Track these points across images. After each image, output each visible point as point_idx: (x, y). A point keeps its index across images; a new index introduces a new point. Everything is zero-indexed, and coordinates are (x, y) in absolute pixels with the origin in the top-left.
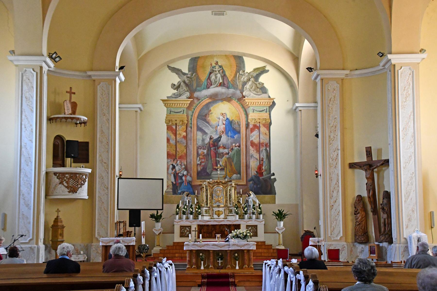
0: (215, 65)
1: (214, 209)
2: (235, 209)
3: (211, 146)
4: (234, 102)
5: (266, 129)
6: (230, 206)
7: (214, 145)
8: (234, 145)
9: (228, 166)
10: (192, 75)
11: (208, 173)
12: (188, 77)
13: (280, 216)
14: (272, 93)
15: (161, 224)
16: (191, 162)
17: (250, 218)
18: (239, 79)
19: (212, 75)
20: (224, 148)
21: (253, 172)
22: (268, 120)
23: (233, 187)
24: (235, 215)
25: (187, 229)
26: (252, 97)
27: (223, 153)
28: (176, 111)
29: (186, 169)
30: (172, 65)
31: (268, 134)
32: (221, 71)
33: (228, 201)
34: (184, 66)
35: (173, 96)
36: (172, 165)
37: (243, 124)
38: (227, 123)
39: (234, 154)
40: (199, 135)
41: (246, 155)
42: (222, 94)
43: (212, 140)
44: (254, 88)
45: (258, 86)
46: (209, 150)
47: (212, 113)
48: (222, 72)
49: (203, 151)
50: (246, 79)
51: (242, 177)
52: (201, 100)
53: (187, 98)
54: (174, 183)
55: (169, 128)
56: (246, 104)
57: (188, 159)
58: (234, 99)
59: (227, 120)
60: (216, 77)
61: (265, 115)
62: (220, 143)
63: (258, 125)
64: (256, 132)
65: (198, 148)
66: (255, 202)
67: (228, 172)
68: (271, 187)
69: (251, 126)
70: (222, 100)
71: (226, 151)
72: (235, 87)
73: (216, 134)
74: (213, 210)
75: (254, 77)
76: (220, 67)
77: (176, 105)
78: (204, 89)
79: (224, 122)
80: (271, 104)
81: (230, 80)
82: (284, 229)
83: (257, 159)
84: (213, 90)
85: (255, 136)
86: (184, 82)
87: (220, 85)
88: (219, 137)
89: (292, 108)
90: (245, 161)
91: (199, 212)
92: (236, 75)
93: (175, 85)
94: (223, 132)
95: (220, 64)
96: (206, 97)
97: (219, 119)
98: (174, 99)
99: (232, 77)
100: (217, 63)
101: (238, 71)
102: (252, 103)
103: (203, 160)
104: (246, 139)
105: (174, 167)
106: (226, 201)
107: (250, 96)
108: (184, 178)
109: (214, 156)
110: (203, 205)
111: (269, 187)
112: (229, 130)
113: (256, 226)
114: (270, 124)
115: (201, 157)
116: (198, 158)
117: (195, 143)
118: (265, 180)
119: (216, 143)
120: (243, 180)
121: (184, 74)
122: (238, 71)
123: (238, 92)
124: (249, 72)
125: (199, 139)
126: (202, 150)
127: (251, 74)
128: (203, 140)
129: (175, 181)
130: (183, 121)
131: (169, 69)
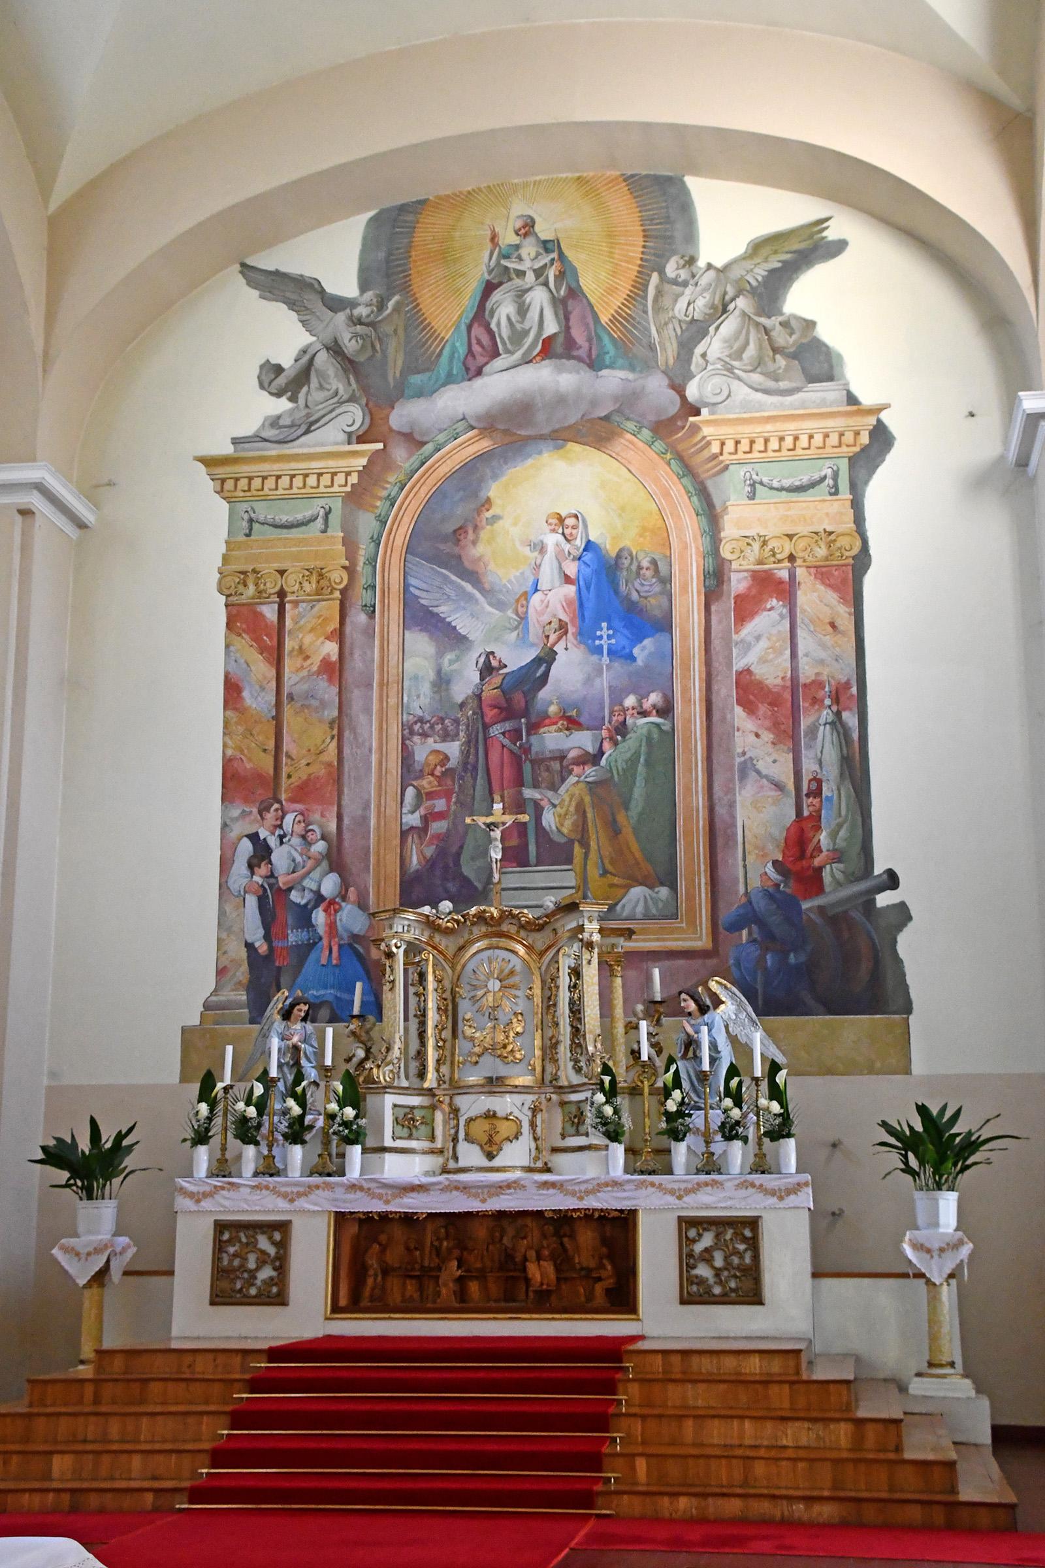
0: (514, 239)
1: (462, 1102)
2: (600, 1098)
3: (490, 714)
4: (635, 446)
5: (832, 597)
6: (576, 1079)
7: (507, 711)
8: (630, 701)
9: (597, 838)
10: (381, 306)
11: (466, 881)
12: (359, 322)
13: (936, 1147)
14: (866, 377)
15: (119, 1209)
16: (365, 819)
17: (710, 1166)
18: (658, 309)
19: (496, 296)
20: (573, 724)
21: (754, 868)
22: (843, 542)
23: (589, 945)
24: (597, 1139)
25: (263, 1243)
26: (746, 406)
27: (562, 757)
28: (284, 518)
29: (335, 861)
30: (267, 261)
31: (846, 622)
32: (551, 274)
33: (564, 1051)
34: (334, 258)
35: (270, 433)
36: (254, 837)
37: (684, 571)
38: (587, 571)
39: (633, 761)
40: (419, 654)
41: (709, 759)
42: (561, 400)
43: (496, 680)
44: (751, 351)
45: (781, 338)
46: (478, 738)
47: (496, 518)
48: (561, 276)
49: (440, 746)
50: (701, 303)
51: (683, 907)
52: (429, 447)
53: (350, 438)
54: (262, 947)
55: (241, 619)
56: (706, 454)
57: (346, 801)
58: (630, 425)
59: (588, 557)
60: (523, 310)
61: (827, 512)
62: (543, 694)
63: (784, 575)
64: (769, 621)
65: (408, 731)
66: (742, 1049)
67: (593, 872)
68: (876, 961)
69: (738, 583)
70: (560, 437)
71: (583, 740)
72: (633, 350)
73: (523, 639)
74: (455, 1111)
75: (753, 291)
76: (547, 246)
77: (284, 482)
78: (450, 380)
79: (572, 569)
80: (865, 439)
81: (604, 319)
82: (966, 1250)
83: (779, 786)
84: (501, 384)
85: (763, 644)
86: (335, 349)
87: (547, 349)
88: (538, 661)
89: (1002, 458)
90: (700, 801)
91: (346, 1124)
92: (641, 285)
93: (279, 369)
94: (563, 627)
95: (544, 231)
96: (461, 426)
97: (541, 548)
98: (274, 451)
99: (617, 301)
100: (527, 228)
101: (652, 263)
102: (744, 445)
103: (440, 805)
104: (708, 663)
105: (262, 852)
106: (550, 1050)
107: (732, 399)
108: (319, 917)
109: (507, 772)
110: (383, 1075)
111: (865, 966)
113: (753, 1223)
114: (862, 561)
115: (427, 783)
116: (410, 792)
117: (393, 701)
118: (836, 919)
119: (519, 699)
120: (692, 922)
121: (336, 304)
122: (652, 263)
123: (656, 386)
124: (719, 264)
126: (432, 743)
127: (737, 272)
128: (442, 682)
129: (267, 937)
130: (321, 575)
131: (250, 283)
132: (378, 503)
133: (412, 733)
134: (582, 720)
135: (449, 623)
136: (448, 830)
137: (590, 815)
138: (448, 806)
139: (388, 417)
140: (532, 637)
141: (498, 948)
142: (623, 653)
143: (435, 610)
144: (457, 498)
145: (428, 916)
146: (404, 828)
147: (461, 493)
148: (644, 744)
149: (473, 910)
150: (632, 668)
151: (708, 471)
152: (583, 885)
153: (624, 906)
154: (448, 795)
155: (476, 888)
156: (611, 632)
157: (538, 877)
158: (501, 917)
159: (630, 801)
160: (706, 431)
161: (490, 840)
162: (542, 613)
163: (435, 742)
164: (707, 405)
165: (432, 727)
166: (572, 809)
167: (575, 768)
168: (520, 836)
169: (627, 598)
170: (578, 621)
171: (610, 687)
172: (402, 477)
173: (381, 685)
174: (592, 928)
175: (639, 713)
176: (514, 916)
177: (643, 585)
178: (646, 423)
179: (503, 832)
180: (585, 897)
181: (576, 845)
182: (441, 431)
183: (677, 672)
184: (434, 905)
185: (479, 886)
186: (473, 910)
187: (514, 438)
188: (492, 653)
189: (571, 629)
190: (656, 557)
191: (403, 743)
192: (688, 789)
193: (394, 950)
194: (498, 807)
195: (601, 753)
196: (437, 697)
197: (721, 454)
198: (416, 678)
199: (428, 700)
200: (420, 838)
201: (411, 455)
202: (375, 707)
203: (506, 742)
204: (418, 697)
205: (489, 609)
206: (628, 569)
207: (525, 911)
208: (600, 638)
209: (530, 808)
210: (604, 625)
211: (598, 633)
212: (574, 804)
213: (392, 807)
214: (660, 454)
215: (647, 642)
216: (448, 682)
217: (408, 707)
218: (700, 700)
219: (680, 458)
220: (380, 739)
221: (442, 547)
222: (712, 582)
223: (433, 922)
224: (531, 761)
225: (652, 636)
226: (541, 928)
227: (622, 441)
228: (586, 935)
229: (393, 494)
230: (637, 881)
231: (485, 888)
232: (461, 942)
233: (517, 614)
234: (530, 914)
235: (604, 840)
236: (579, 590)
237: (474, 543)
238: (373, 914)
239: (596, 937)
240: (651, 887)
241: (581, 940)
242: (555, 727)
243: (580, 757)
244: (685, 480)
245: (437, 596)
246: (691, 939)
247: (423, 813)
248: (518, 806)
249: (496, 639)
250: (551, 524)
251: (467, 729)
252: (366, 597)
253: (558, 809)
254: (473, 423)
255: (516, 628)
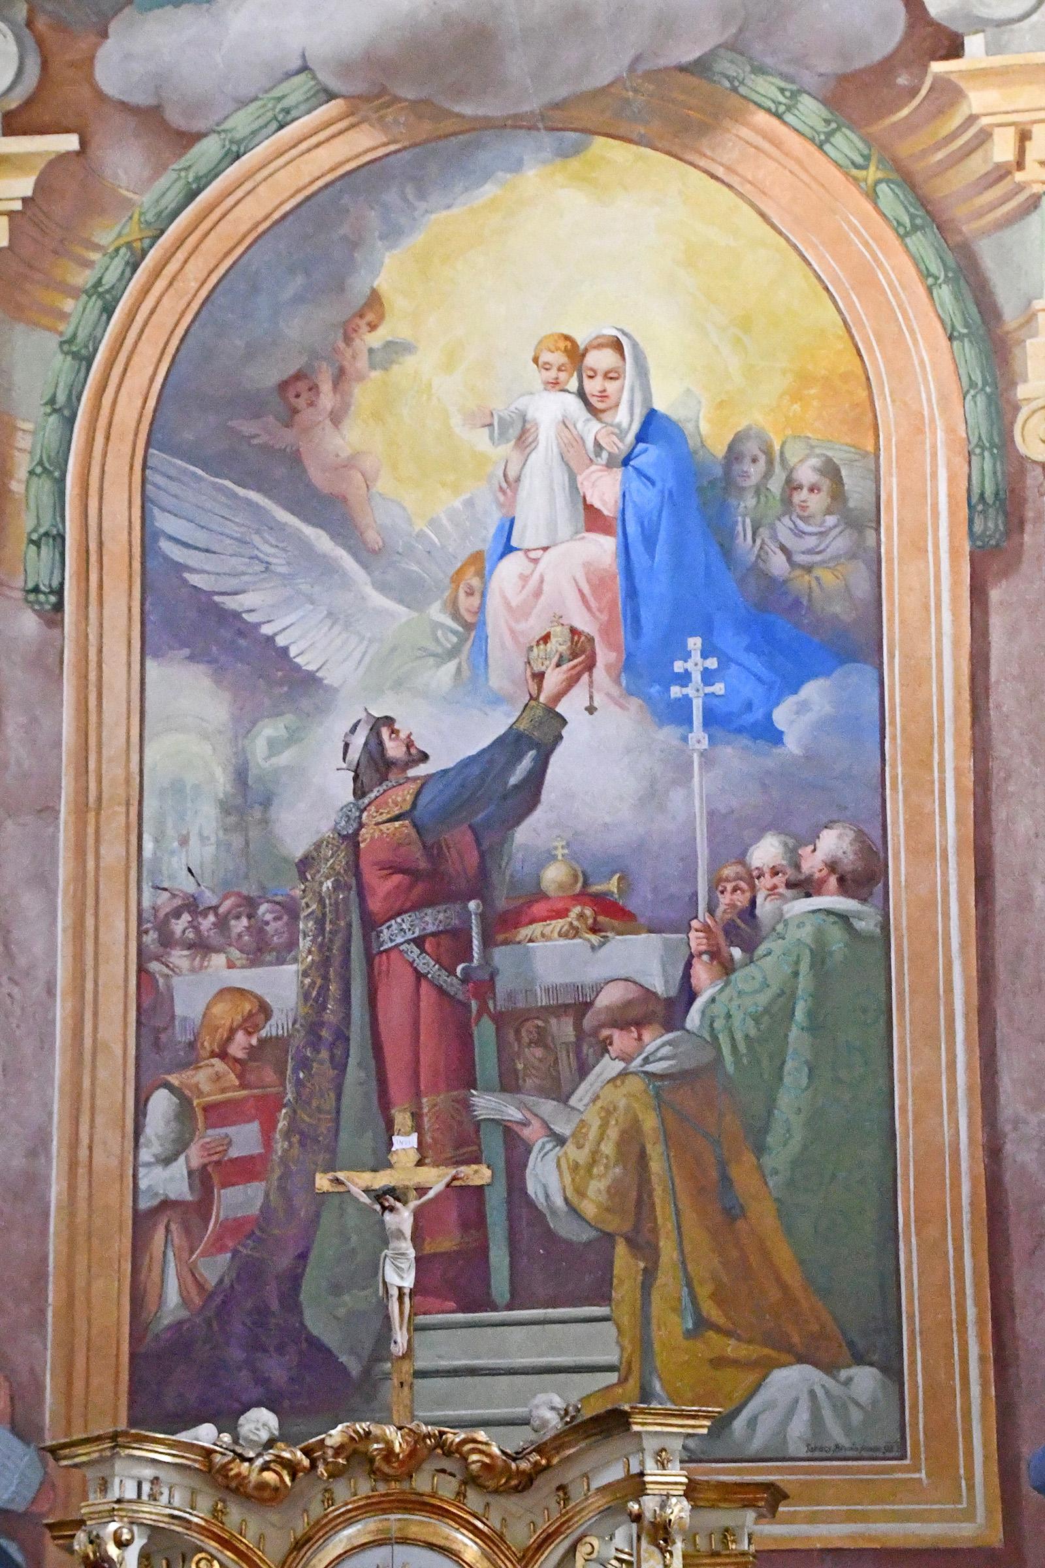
8: (767, 852)
20: (609, 913)
38: (646, 497)
39: (777, 1014)
40: (188, 721)
46: (347, 961)
47: (396, 349)
49: (243, 978)
51: (919, 1423)
52: (209, 149)
56: (976, 165)
58: (766, 88)
59: (649, 456)
62: (528, 833)
65: (156, 938)
67: (670, 1326)
70: (573, 122)
71: (637, 960)
79: (605, 489)
88: (512, 743)
90: (962, 1126)
94: (581, 652)
97: (522, 434)
103: (244, 1139)
104: (981, 747)
112: (690, 617)
115: (208, 1080)
116: (161, 1103)
117: (113, 852)
119: (459, 839)
120: (944, 1466)
125: (177, 788)
126: (221, 970)
132: (68, 305)
133: (167, 941)
134: (633, 904)
135: (270, 639)
136: (266, 1208)
137: (656, 1166)
138: (268, 1141)
139: (89, 61)
140: (497, 680)
141: (404, 1541)
142: (749, 718)
143: (231, 603)
144: (289, 293)
145: (208, 1453)
146: (144, 1204)
147: (300, 280)
148: (804, 967)
149: (336, 1435)
150: (772, 760)
151: (980, 215)
152: (640, 1359)
153: (752, 1422)
154: (266, 1110)
155: (343, 1370)
156: (712, 663)
157: (518, 1340)
158: (412, 1454)
159: (765, 1130)
160: (979, 100)
161: (384, 1238)
162: (520, 613)
163: (231, 965)
164: (981, 25)
165: (222, 924)
166: (608, 1148)
167: (617, 1035)
168: (465, 1226)
169: (758, 571)
170: (621, 634)
171: (711, 814)
172: (133, 232)
173: (81, 809)
174: (666, 1480)
175: (789, 885)
176: (449, 1451)
177: (800, 534)
178: (808, 79)
179: (417, 1214)
180: (646, 1395)
181: (621, 1249)
182: (243, 103)
183: (896, 771)
184: (227, 1420)
185: (354, 1368)
186: (336, 1435)
187: (448, 125)
188: (388, 721)
189: (604, 656)
190: (837, 457)
191: (141, 970)
192: (927, 1093)
193: (113, 1551)
194: (405, 1143)
195: (689, 994)
196: (237, 841)
197: (1020, 165)
198: (177, 788)
199: (210, 850)
200: (187, 1230)
201: (160, 169)
202: (63, 872)
203: (426, 964)
204: (184, 841)
205: (378, 600)
206: (760, 490)
207: (481, 1435)
208: (684, 678)
209: (493, 1143)
210: (695, 643)
211: (679, 666)
212: (613, 1133)
213: (109, 1145)
214: (851, 168)
215: (812, 690)
216: (266, 803)
217: (156, 872)
218: (959, 852)
219: (906, 179)
220: (78, 958)
221: (248, 428)
222: (992, 524)
223: (225, 1468)
224: (499, 1019)
225: (827, 674)
226: (526, 1482)
227: (745, 132)
228: (650, 1504)
229: (110, 279)
230: (789, 1349)
231: (367, 1372)
232: (301, 1526)
233: (456, 615)
234: (494, 1443)
235: (695, 1232)
236: (626, 549)
237: (336, 418)
238: (53, 1451)
239: (679, 1510)
240: (830, 1369)
241: (637, 1518)
242: (559, 924)
243: (628, 1004)
244: (917, 242)
245: (236, 563)
246: (943, 1517)
247: (195, 1163)
248: (460, 1141)
249: (398, 685)
250: (547, 367)
251: (321, 928)
252: (38, 566)
253: (570, 1147)
254: (334, 84)
255: (453, 653)
